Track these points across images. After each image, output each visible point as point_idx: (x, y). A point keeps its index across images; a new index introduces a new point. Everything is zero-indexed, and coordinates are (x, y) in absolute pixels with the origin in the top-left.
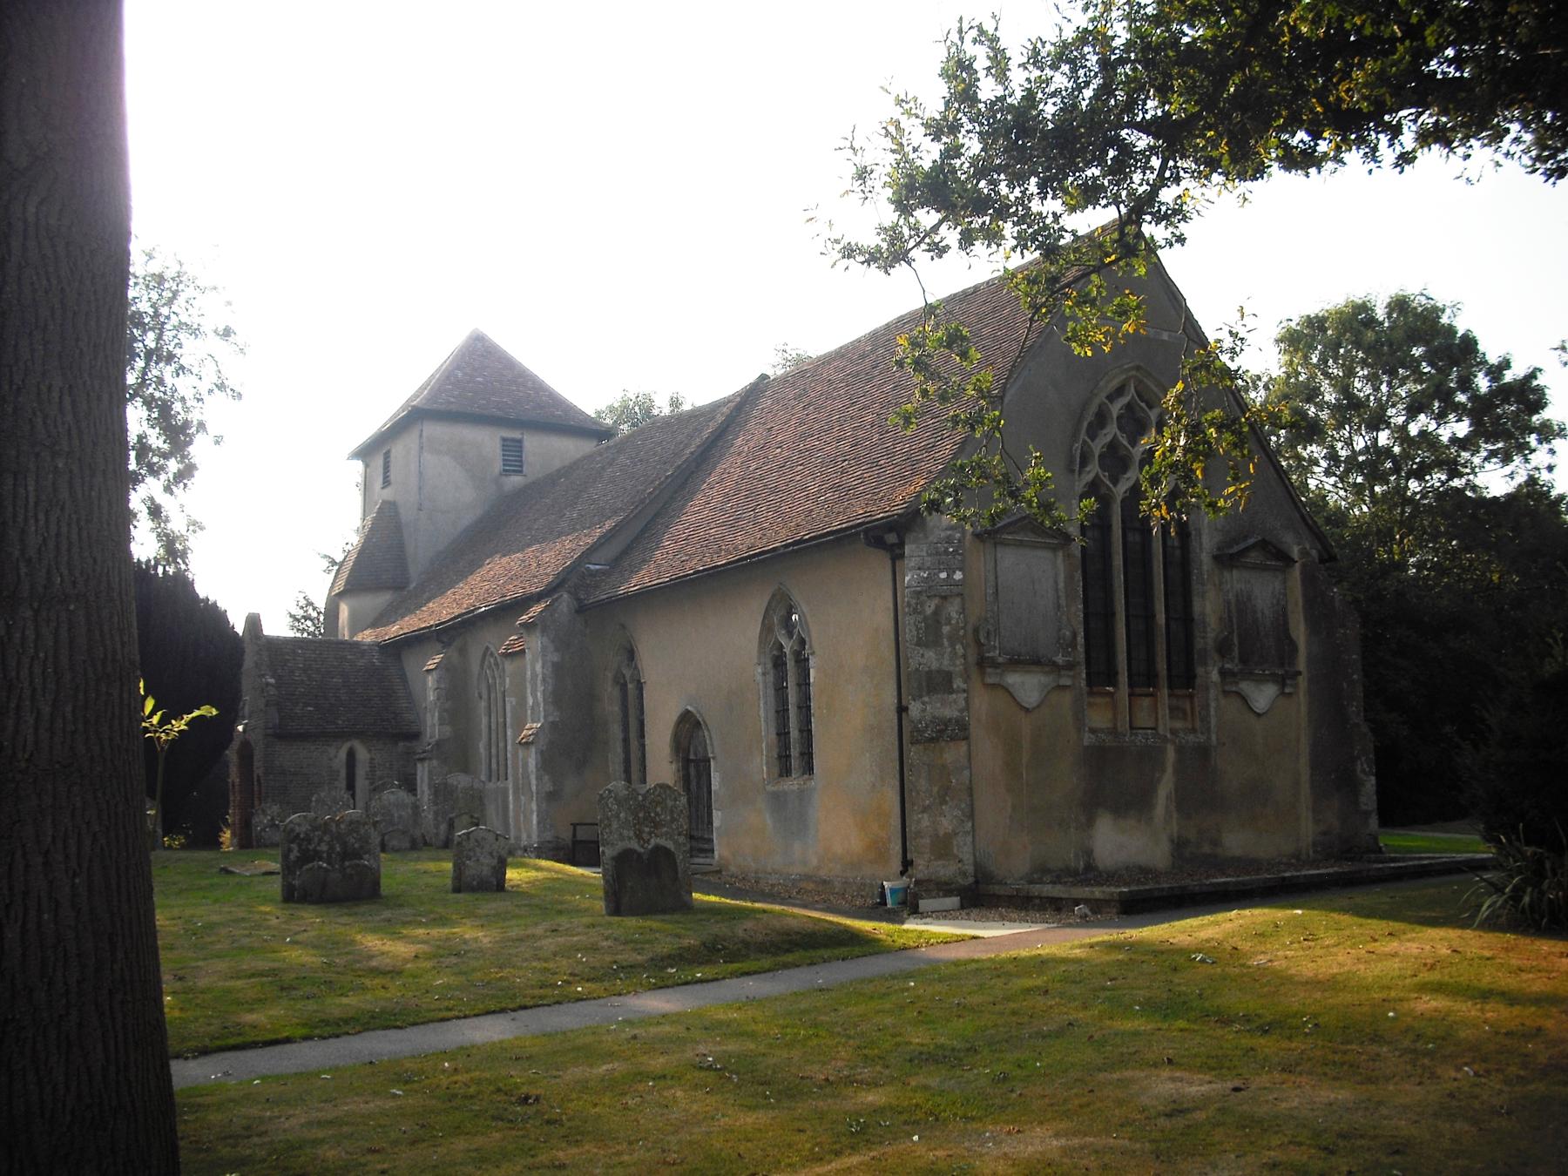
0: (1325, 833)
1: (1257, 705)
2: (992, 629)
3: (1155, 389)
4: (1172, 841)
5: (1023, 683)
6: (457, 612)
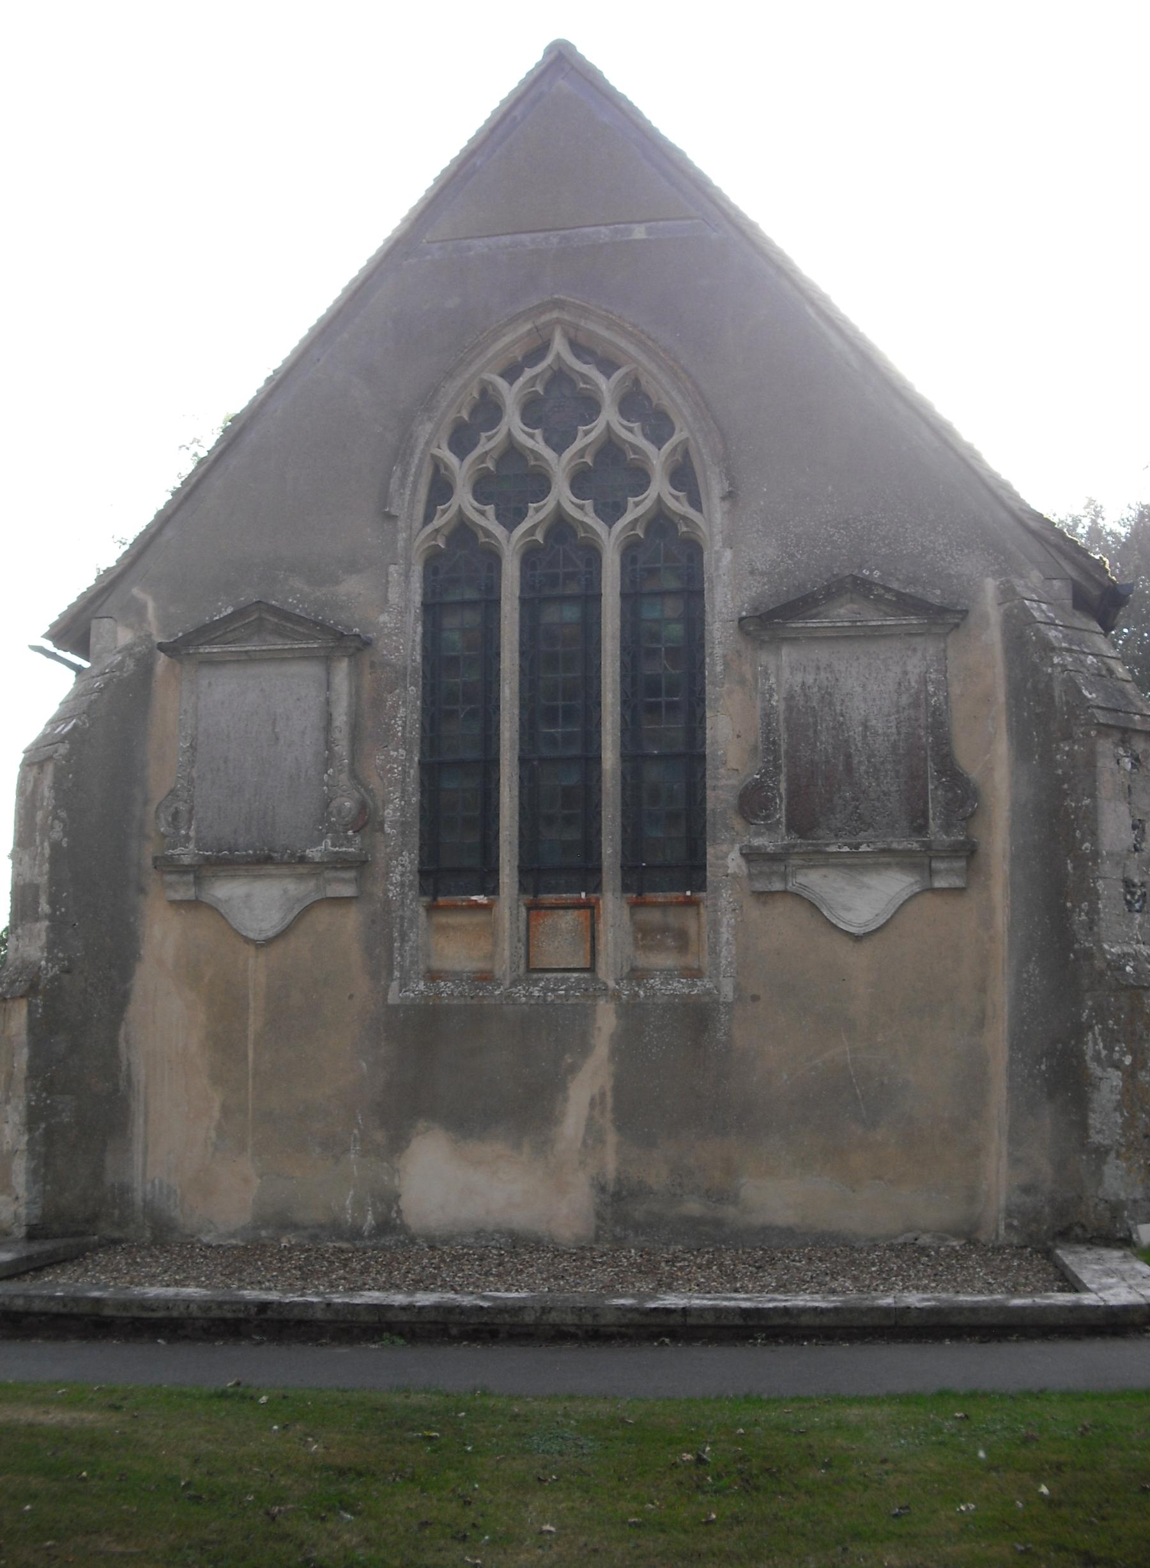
0: (1027, 1190)
1: (848, 916)
2: (183, 807)
3: (606, 334)
4: (603, 1189)
5: (248, 896)
6: (416, 829)
